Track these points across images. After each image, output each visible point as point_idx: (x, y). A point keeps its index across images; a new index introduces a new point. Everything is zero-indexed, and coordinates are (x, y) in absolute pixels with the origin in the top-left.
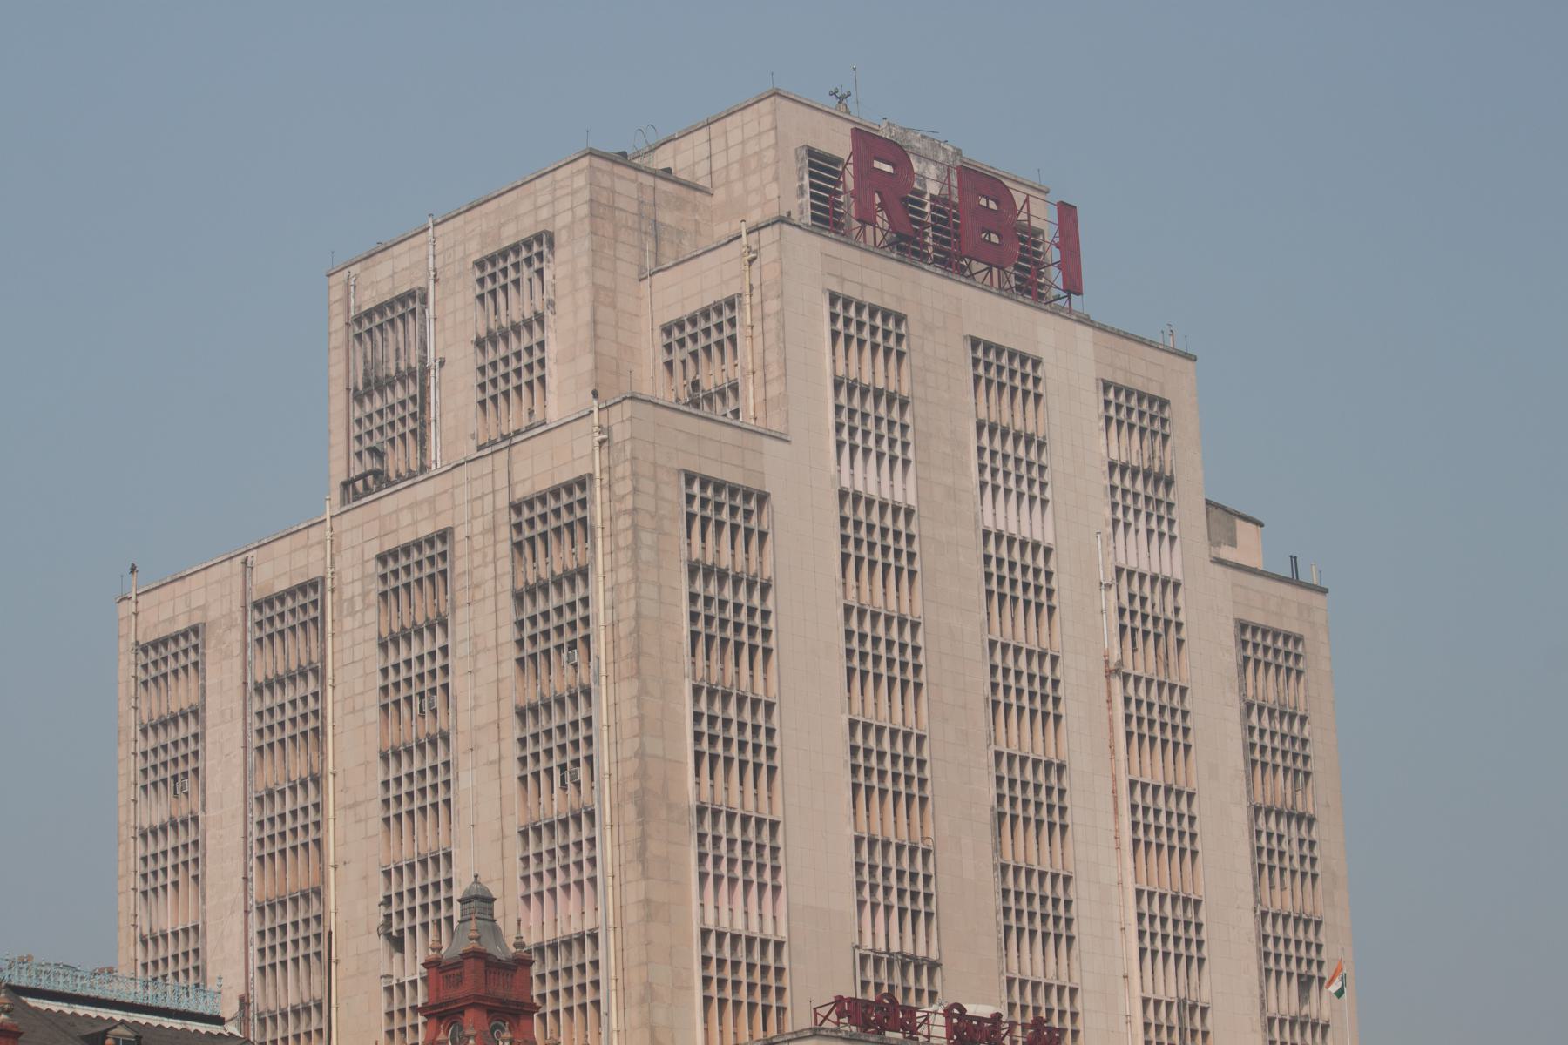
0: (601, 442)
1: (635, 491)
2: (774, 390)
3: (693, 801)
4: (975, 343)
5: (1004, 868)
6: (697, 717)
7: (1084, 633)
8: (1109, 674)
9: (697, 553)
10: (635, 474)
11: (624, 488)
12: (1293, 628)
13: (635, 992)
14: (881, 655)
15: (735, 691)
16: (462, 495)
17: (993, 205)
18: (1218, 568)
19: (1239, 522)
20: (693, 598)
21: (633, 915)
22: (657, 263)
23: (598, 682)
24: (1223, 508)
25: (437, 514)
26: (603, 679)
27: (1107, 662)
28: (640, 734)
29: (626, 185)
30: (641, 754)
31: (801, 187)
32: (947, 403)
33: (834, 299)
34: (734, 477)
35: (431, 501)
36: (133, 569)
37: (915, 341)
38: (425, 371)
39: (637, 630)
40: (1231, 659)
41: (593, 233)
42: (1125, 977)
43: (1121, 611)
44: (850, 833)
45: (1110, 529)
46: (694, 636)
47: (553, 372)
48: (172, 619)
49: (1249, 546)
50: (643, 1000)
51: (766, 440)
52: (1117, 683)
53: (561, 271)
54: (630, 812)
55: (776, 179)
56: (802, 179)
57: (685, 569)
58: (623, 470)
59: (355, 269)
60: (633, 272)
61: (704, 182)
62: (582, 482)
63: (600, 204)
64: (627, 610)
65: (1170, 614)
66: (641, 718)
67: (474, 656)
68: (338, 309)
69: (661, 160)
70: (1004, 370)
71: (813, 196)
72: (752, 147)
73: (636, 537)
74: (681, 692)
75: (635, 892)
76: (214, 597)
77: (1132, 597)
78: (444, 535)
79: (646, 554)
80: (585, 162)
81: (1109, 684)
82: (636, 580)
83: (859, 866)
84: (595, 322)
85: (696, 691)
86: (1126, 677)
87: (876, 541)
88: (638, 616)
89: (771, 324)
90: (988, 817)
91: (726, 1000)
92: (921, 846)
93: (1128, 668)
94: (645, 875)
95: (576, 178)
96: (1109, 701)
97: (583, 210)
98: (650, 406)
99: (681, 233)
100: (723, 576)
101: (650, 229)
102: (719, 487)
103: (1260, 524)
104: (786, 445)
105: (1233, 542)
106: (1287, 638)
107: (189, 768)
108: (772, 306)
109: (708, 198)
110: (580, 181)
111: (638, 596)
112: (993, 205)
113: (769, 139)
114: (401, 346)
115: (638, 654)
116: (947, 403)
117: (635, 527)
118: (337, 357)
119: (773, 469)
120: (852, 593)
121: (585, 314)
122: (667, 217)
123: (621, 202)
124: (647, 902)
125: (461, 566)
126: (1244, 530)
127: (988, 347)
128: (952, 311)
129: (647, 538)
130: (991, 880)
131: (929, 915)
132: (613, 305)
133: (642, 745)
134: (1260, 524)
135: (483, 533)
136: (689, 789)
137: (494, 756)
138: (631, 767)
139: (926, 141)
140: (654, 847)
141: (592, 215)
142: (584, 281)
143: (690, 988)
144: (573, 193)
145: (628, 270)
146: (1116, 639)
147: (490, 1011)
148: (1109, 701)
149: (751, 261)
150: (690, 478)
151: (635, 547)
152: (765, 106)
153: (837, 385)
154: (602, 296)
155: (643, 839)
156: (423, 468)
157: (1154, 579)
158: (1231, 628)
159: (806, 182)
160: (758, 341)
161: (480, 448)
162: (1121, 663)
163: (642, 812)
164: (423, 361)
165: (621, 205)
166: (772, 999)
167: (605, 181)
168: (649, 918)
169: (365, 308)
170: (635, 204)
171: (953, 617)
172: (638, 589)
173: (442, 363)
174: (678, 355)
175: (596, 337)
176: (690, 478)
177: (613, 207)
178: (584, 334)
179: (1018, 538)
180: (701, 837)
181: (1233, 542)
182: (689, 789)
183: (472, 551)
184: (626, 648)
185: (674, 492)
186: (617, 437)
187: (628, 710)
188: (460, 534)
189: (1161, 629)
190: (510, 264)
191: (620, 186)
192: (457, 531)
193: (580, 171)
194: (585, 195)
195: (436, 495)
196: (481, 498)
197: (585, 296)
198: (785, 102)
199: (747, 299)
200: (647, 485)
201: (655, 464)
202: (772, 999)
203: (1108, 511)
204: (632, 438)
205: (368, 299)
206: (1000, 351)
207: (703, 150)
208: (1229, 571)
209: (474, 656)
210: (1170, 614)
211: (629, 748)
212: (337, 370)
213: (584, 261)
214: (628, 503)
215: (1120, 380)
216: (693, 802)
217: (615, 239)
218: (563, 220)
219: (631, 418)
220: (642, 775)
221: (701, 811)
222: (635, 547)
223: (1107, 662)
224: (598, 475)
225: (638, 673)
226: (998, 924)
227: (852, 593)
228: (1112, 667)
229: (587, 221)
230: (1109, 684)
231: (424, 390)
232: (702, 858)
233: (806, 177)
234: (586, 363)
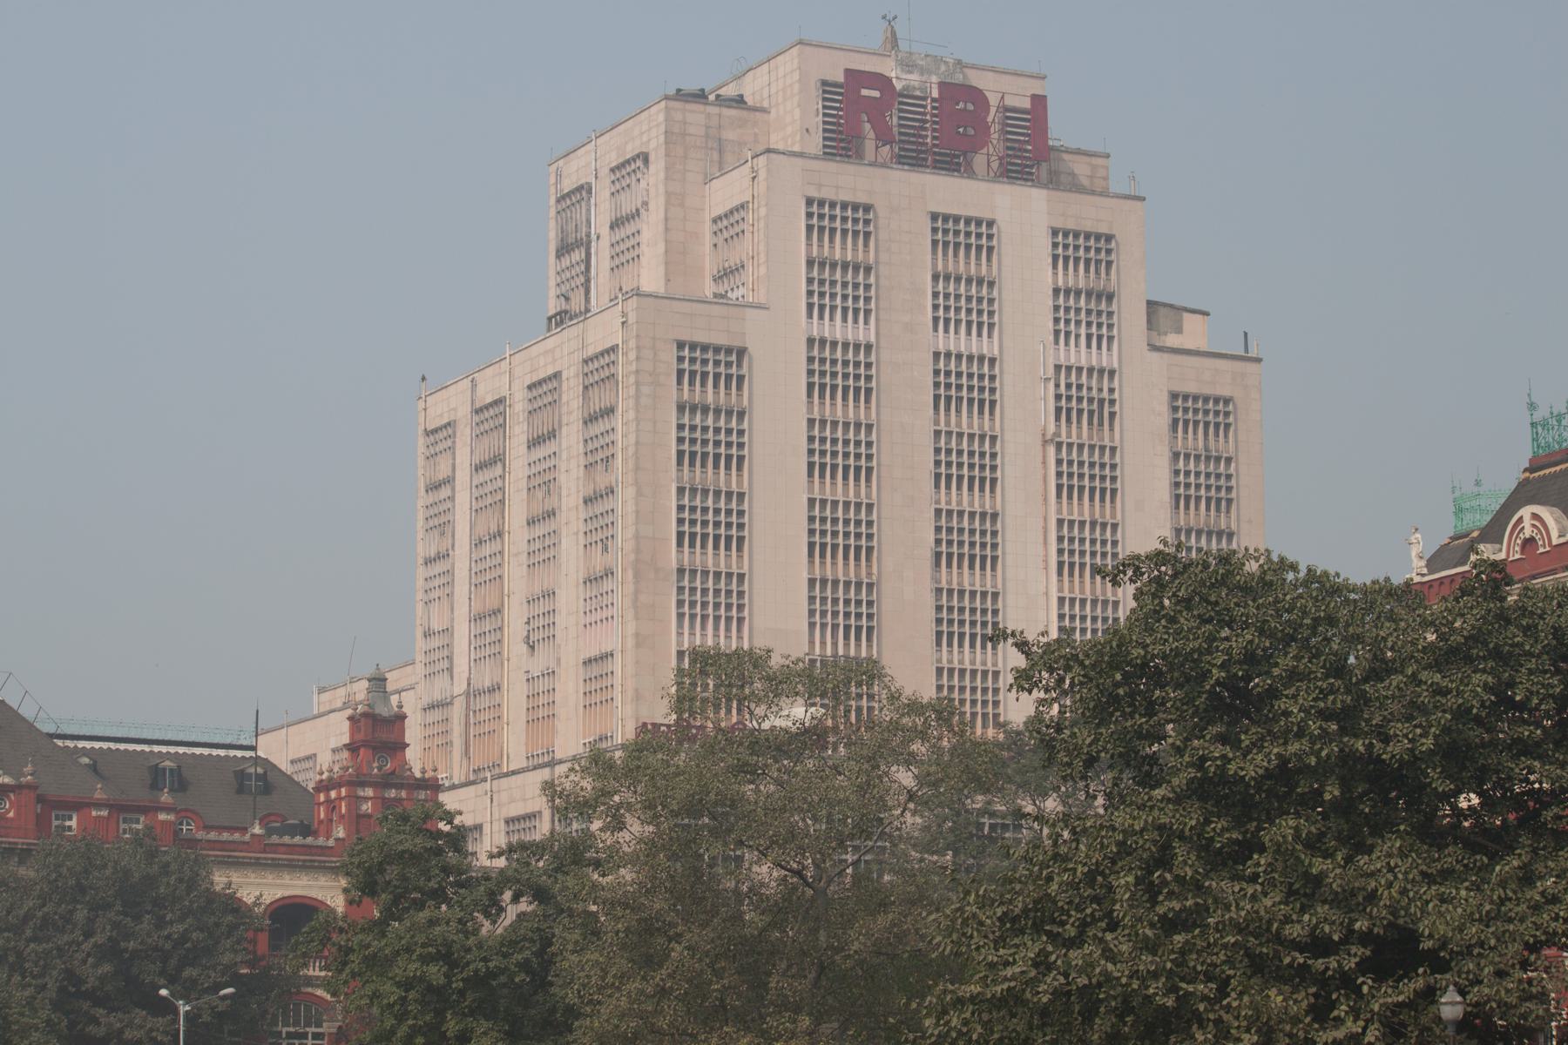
4: (934, 217)
8: (1045, 442)
12: (1225, 392)
13: (630, 693)
17: (970, 107)
18: (1156, 355)
19: (1186, 315)
21: (630, 642)
24: (1171, 306)
29: (696, 116)
32: (906, 263)
33: (809, 202)
34: (721, 340)
36: (424, 379)
37: (881, 222)
38: (589, 243)
39: (636, 452)
40: (1164, 419)
41: (667, 155)
43: (1058, 397)
44: (805, 576)
46: (680, 454)
47: (644, 249)
48: (441, 415)
49: (1194, 333)
54: (630, 574)
58: (632, 344)
59: (561, 163)
62: (614, 349)
66: (637, 512)
68: (553, 190)
69: (730, 91)
70: (962, 236)
73: (637, 390)
76: (452, 404)
81: (1044, 451)
84: (666, 219)
85: (681, 490)
86: (1059, 445)
87: (839, 374)
88: (637, 443)
93: (1064, 438)
94: (637, 618)
95: (658, 114)
96: (1044, 463)
97: (662, 138)
101: (715, 145)
103: (1206, 314)
105: (1179, 330)
106: (1217, 401)
110: (661, 117)
112: (970, 107)
116: (906, 263)
118: (552, 224)
119: (755, 333)
121: (662, 215)
122: (729, 135)
123: (692, 130)
126: (1189, 320)
127: (946, 218)
128: (908, 198)
129: (645, 390)
130: (929, 600)
131: (870, 629)
134: (1206, 314)
146: (1052, 418)
147: (374, 749)
148: (1044, 463)
150: (681, 345)
152: (795, 50)
153: (810, 263)
154: (674, 199)
155: (637, 592)
156: (587, 310)
157: (1091, 370)
158: (1165, 398)
163: (637, 575)
164: (588, 235)
167: (678, 116)
168: (638, 645)
176: (681, 345)
177: (684, 134)
178: (661, 227)
179: (966, 353)
180: (680, 589)
181: (1179, 330)
184: (631, 464)
188: (564, 376)
190: (631, 166)
198: (808, 49)
201: (654, 338)
205: (567, 185)
206: (957, 219)
208: (1166, 356)
209: (568, 460)
210: (1105, 394)
212: (552, 235)
216: (674, 565)
218: (653, 145)
220: (637, 551)
221: (681, 571)
228: (1049, 437)
230: (1044, 451)
231: (588, 255)
232: (680, 603)
234: (661, 247)
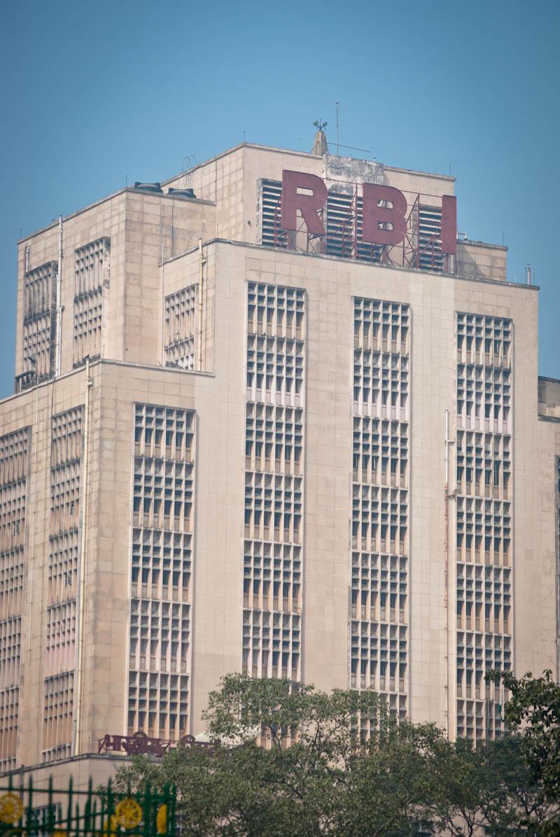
0: (89, 386)
1: (102, 417)
2: (210, 344)
3: (129, 597)
5: (355, 624)
6: (136, 547)
7: (430, 479)
8: (448, 498)
9: (142, 450)
10: (102, 408)
11: (97, 415)
13: (88, 708)
14: (273, 503)
15: (163, 530)
16: (36, 407)
20: (137, 477)
21: (89, 664)
22: (173, 254)
23: (81, 527)
25: (26, 417)
26: (84, 526)
27: (447, 491)
28: (98, 559)
29: (152, 207)
30: (97, 571)
31: (258, 204)
32: (332, 339)
33: (251, 286)
35: (24, 408)
37: (312, 305)
38: (55, 313)
39: (99, 498)
41: (127, 241)
42: (447, 687)
44: (241, 608)
45: (455, 407)
50: (90, 715)
51: (197, 377)
52: (453, 504)
53: (113, 262)
55: (242, 201)
56: (259, 199)
57: (133, 461)
58: (97, 404)
59: (29, 242)
60: (156, 261)
61: (212, 198)
63: (132, 222)
64: (95, 486)
65: (501, 457)
66: (98, 550)
67: (36, 503)
68: (21, 265)
71: (265, 210)
72: (233, 179)
73: (101, 445)
74: (126, 533)
75: (90, 651)
77: (469, 449)
78: (27, 429)
79: (106, 454)
80: (124, 195)
81: (447, 505)
82: (100, 469)
83: (246, 629)
84: (125, 296)
86: (460, 500)
87: (274, 434)
88: (100, 490)
89: (210, 304)
90: (346, 593)
91: (145, 713)
92: (292, 614)
93: (464, 494)
96: (447, 515)
97: (123, 226)
98: (115, 366)
99: (191, 233)
100: (159, 463)
101: (169, 233)
102: (159, 410)
104: (212, 379)
107: (21, 518)
108: (211, 293)
109: (212, 208)
110: (122, 207)
111: (100, 480)
113: (240, 175)
114: (45, 295)
115: (99, 512)
116: (332, 339)
117: (101, 439)
119: (201, 396)
120: (253, 464)
122: (181, 224)
123: (148, 219)
124: (95, 657)
125: (34, 450)
127: (367, 302)
130: (346, 632)
131: (295, 656)
132: (139, 285)
133: (97, 566)
135: (43, 431)
136: (127, 590)
137: (41, 564)
138: (92, 578)
139: (355, 162)
140: (101, 625)
141: (126, 230)
142: (122, 270)
143: (121, 706)
144: (119, 214)
145: (150, 261)
146: (454, 477)
148: (447, 515)
149: (203, 264)
150: (139, 407)
151: (101, 450)
155: (96, 621)
156: (52, 373)
157: (488, 436)
159: (261, 202)
160: (204, 313)
161: (75, 366)
162: (458, 491)
163: (96, 605)
164: (54, 307)
165: (148, 221)
166: (178, 711)
168: (96, 666)
169: (33, 268)
170: (159, 219)
171: (329, 477)
172: (101, 475)
173: (63, 310)
174: (172, 316)
175: (126, 305)
176: (139, 407)
177: (142, 223)
178: (121, 303)
179: (381, 419)
180: (134, 618)
182: (127, 590)
183: (38, 441)
184: (94, 509)
185: (129, 415)
186: (96, 385)
187: (93, 546)
188: (35, 429)
189: (492, 467)
191: (148, 209)
192: (33, 428)
193: (122, 201)
194: (123, 217)
195: (26, 405)
196: (43, 410)
197: (122, 279)
199: (200, 287)
200: (110, 413)
201: (116, 400)
202: (178, 711)
203: (455, 395)
204: (102, 386)
207: (213, 176)
209: (36, 503)
210: (501, 457)
211: (92, 567)
213: (122, 258)
214: (98, 425)
215: (474, 310)
217: (143, 243)
219: (102, 374)
220: (98, 583)
222: (101, 450)
223: (447, 491)
224: (87, 406)
225: (98, 525)
226: (348, 658)
227: (253, 464)
228: (451, 493)
229: (124, 233)
230: (447, 505)
232: (133, 630)
233: (261, 198)
234: (120, 321)
